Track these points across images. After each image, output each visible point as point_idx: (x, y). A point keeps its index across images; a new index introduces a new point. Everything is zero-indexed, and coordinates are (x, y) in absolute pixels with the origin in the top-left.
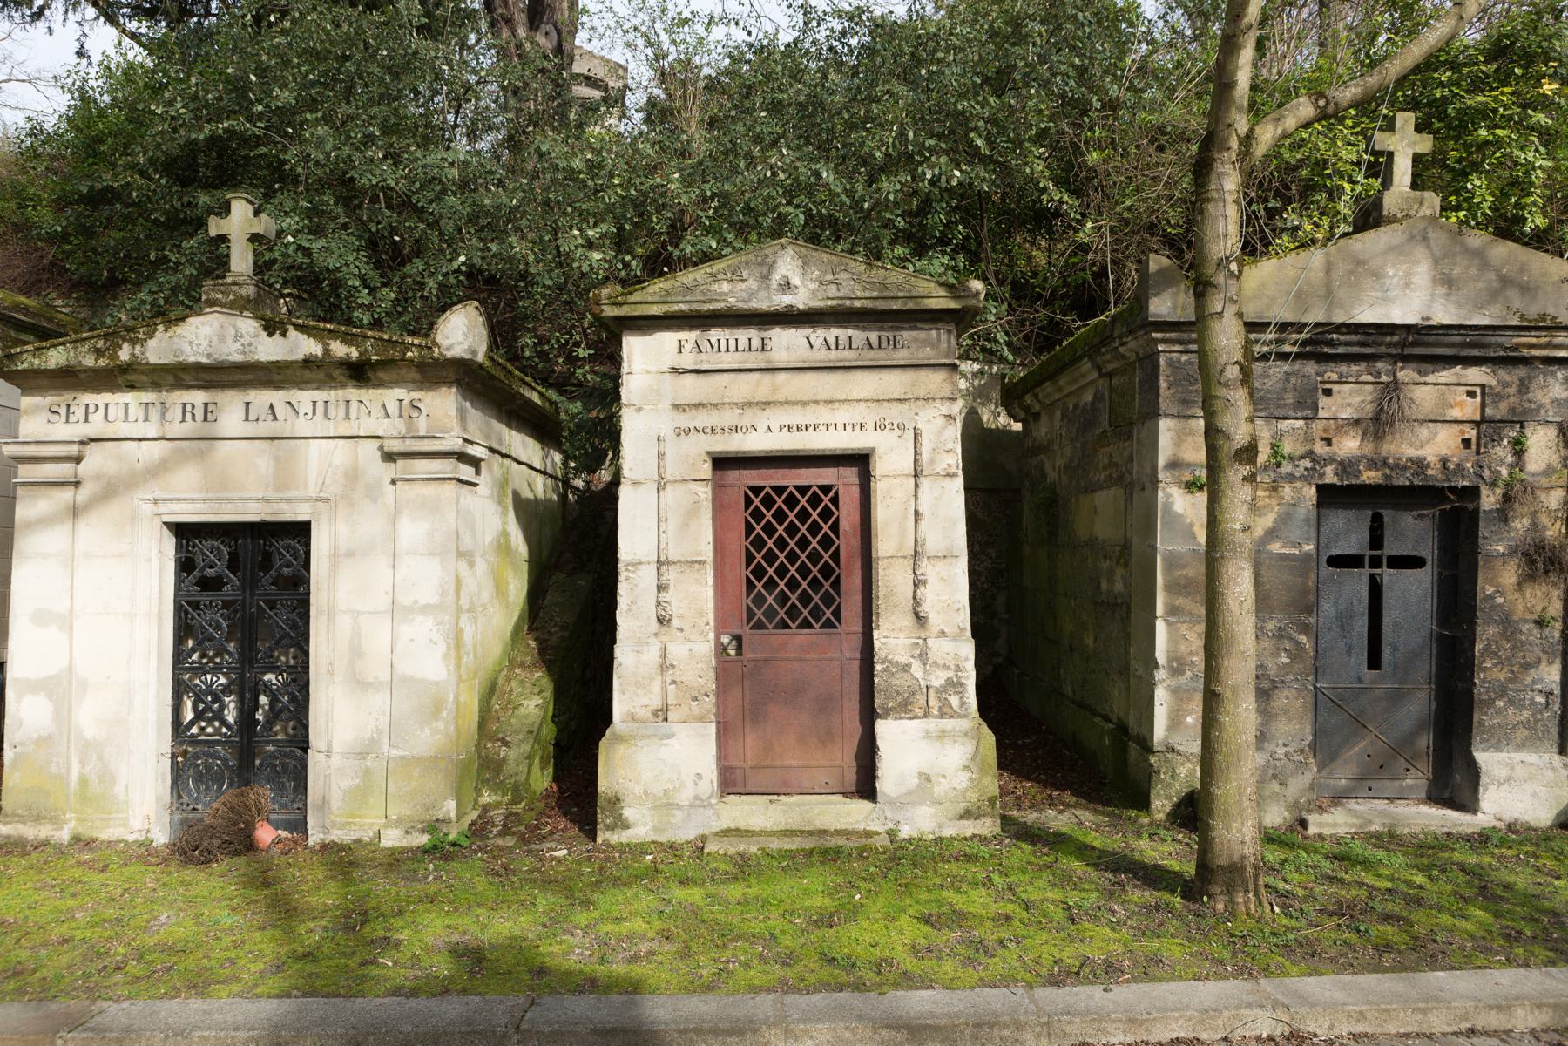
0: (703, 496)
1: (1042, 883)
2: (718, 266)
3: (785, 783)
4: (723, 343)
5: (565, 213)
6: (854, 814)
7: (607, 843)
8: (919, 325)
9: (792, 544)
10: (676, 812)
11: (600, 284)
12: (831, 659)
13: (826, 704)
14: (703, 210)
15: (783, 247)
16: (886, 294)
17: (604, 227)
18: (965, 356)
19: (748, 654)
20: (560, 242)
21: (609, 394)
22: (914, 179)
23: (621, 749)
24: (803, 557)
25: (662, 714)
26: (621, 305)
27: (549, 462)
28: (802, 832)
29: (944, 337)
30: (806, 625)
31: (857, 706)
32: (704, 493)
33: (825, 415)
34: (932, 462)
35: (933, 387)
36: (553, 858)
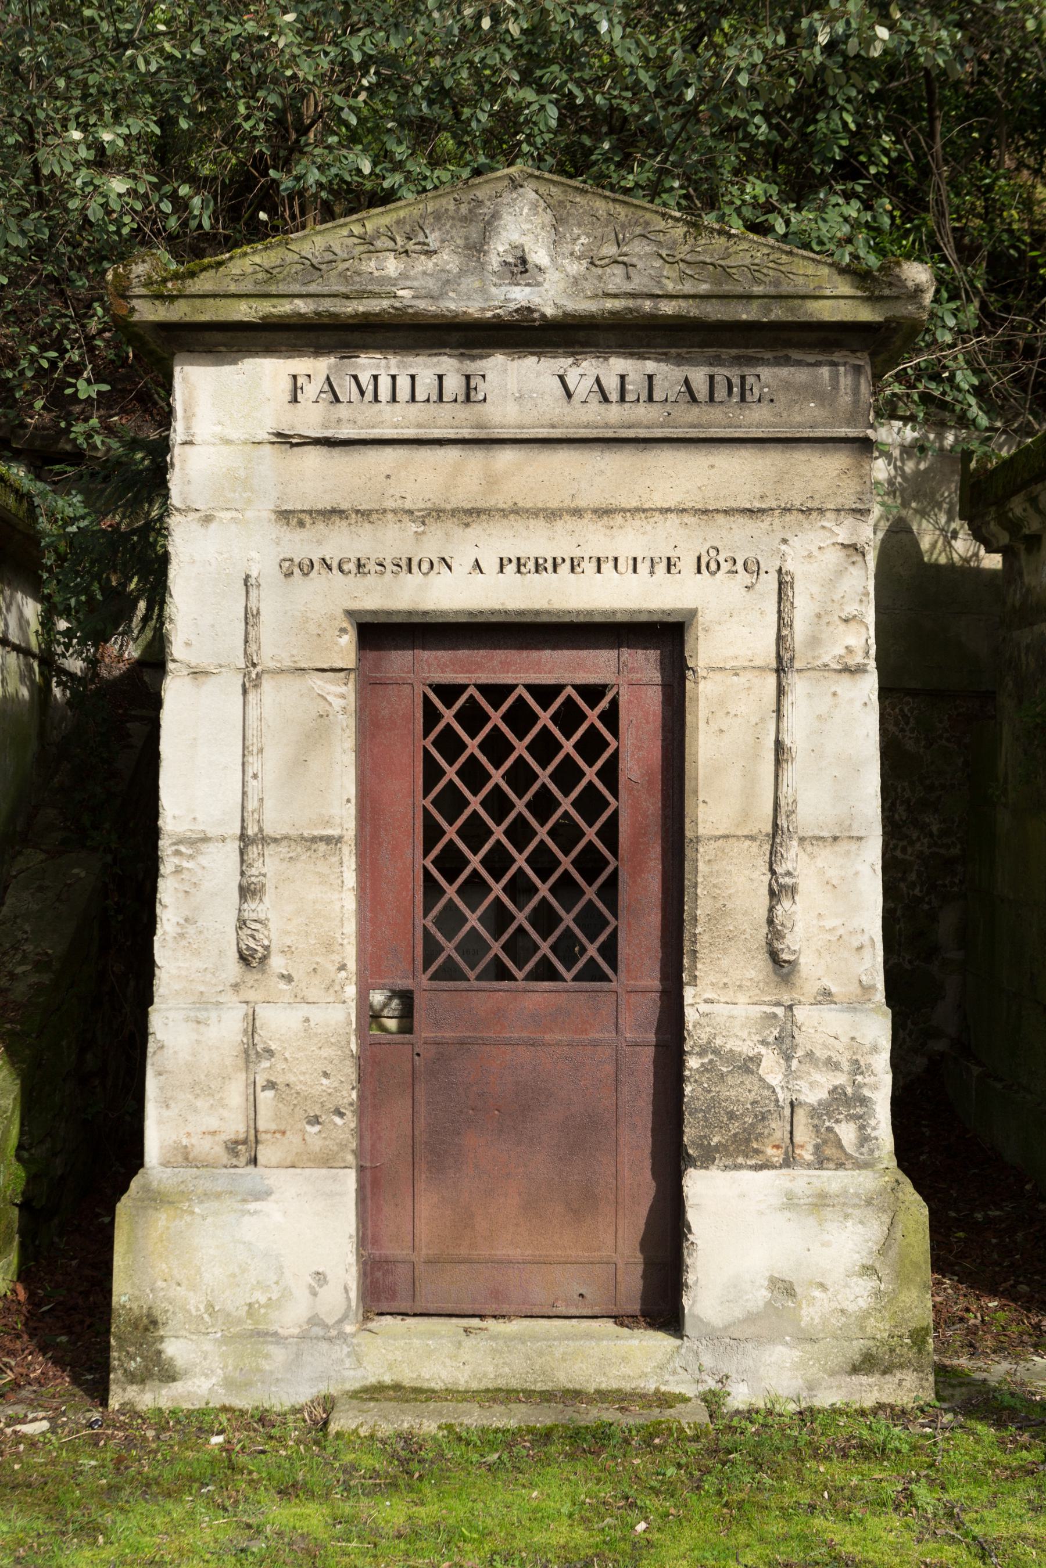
0: (337, 703)
1: (1014, 1504)
2: (378, 220)
3: (496, 1295)
4: (384, 383)
5: (52, 89)
6: (639, 1359)
7: (129, 1410)
8: (795, 355)
9: (520, 805)
10: (272, 1349)
11: (121, 251)
12: (595, 1044)
13: (583, 1135)
14: (346, 93)
15: (515, 184)
16: (727, 288)
17: (135, 125)
18: (889, 411)
19: (424, 1031)
20: (41, 154)
21: (146, 477)
22: (791, 39)
23: (161, 1220)
24: (542, 833)
25: (246, 1149)
26: (172, 298)
27: (12, 620)
28: (529, 1394)
29: (845, 381)
30: (545, 972)
31: (646, 1141)
32: (340, 696)
33: (594, 539)
34: (814, 641)
35: (821, 486)
36: (19, 1438)
